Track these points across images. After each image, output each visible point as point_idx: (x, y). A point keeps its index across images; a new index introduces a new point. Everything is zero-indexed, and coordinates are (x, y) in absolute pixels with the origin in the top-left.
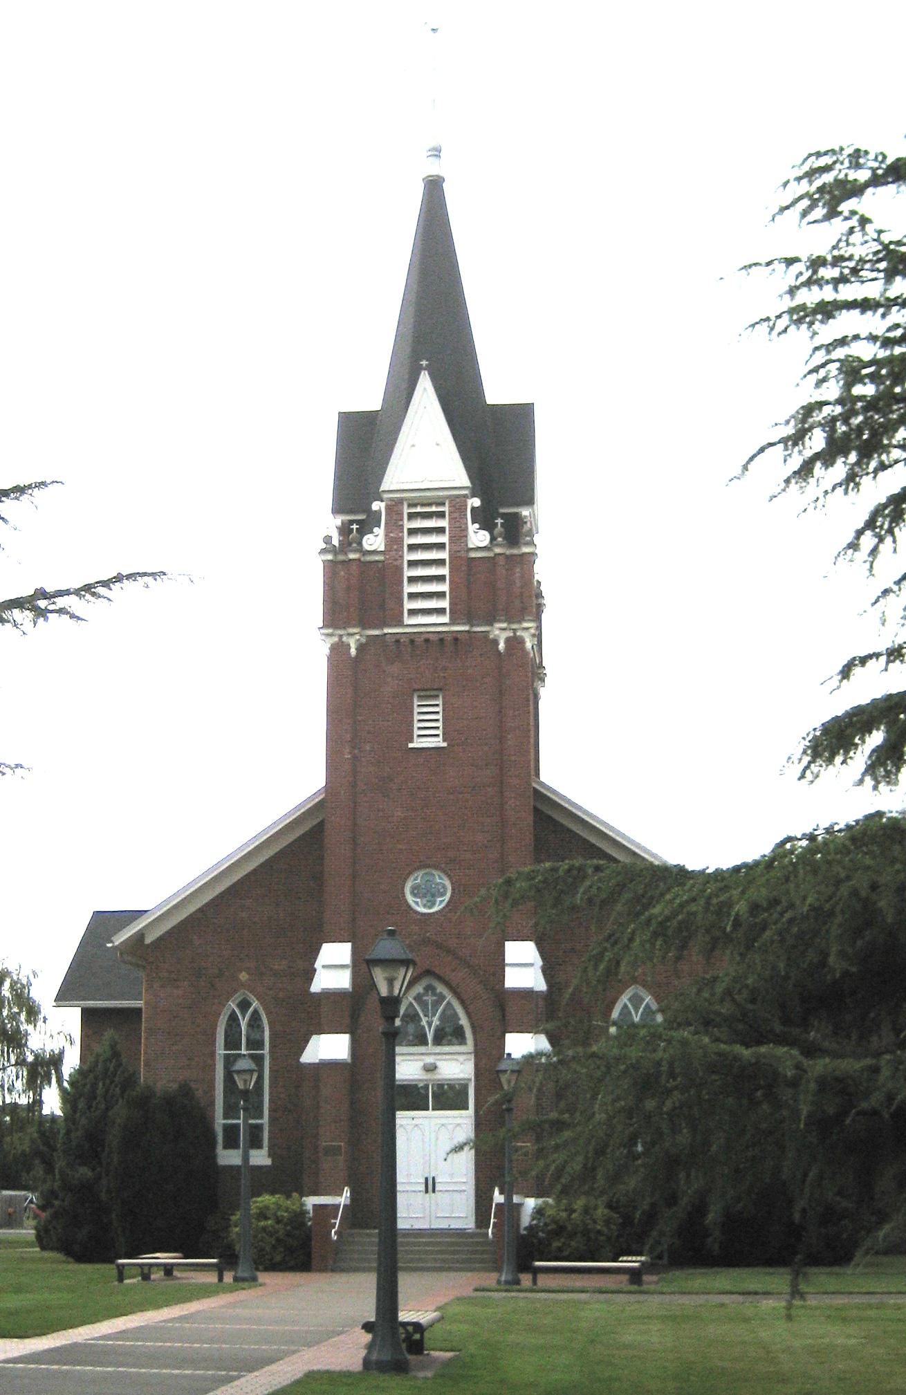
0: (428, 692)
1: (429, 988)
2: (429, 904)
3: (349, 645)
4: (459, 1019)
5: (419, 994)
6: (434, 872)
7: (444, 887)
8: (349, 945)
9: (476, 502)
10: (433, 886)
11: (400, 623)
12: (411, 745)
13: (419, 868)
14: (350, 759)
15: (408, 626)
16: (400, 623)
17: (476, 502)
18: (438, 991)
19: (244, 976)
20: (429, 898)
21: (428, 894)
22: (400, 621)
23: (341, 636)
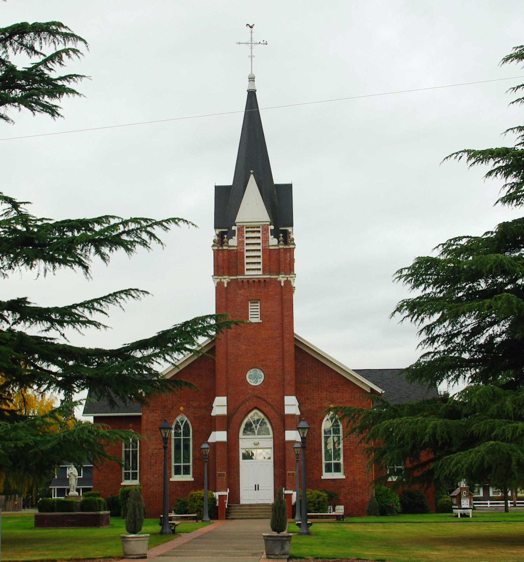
0: (254, 301)
3: (224, 283)
6: (258, 370)
7: (261, 375)
9: (272, 227)
19: (182, 409)
21: (256, 378)
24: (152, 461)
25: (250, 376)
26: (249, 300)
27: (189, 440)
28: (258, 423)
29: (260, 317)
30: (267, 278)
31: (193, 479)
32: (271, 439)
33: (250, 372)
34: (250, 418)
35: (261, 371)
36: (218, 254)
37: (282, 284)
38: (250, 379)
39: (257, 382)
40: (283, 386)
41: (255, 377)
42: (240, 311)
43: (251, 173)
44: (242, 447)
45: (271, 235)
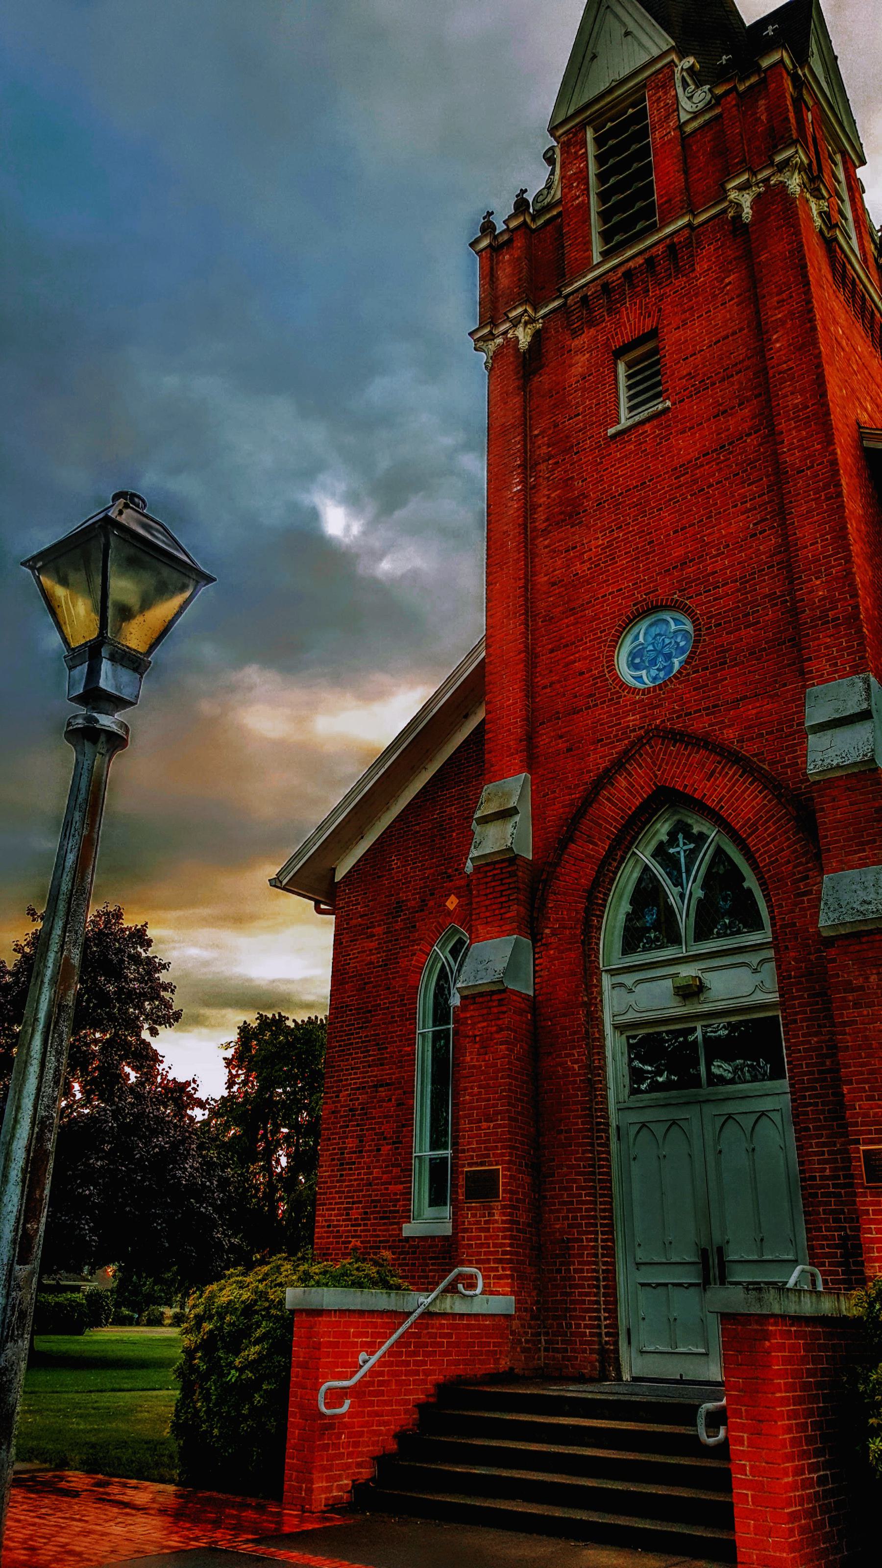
4: (743, 879)
6: (667, 616)
8: (749, 19)
10: (667, 641)
18: (695, 830)
19: (452, 903)
25: (633, 655)
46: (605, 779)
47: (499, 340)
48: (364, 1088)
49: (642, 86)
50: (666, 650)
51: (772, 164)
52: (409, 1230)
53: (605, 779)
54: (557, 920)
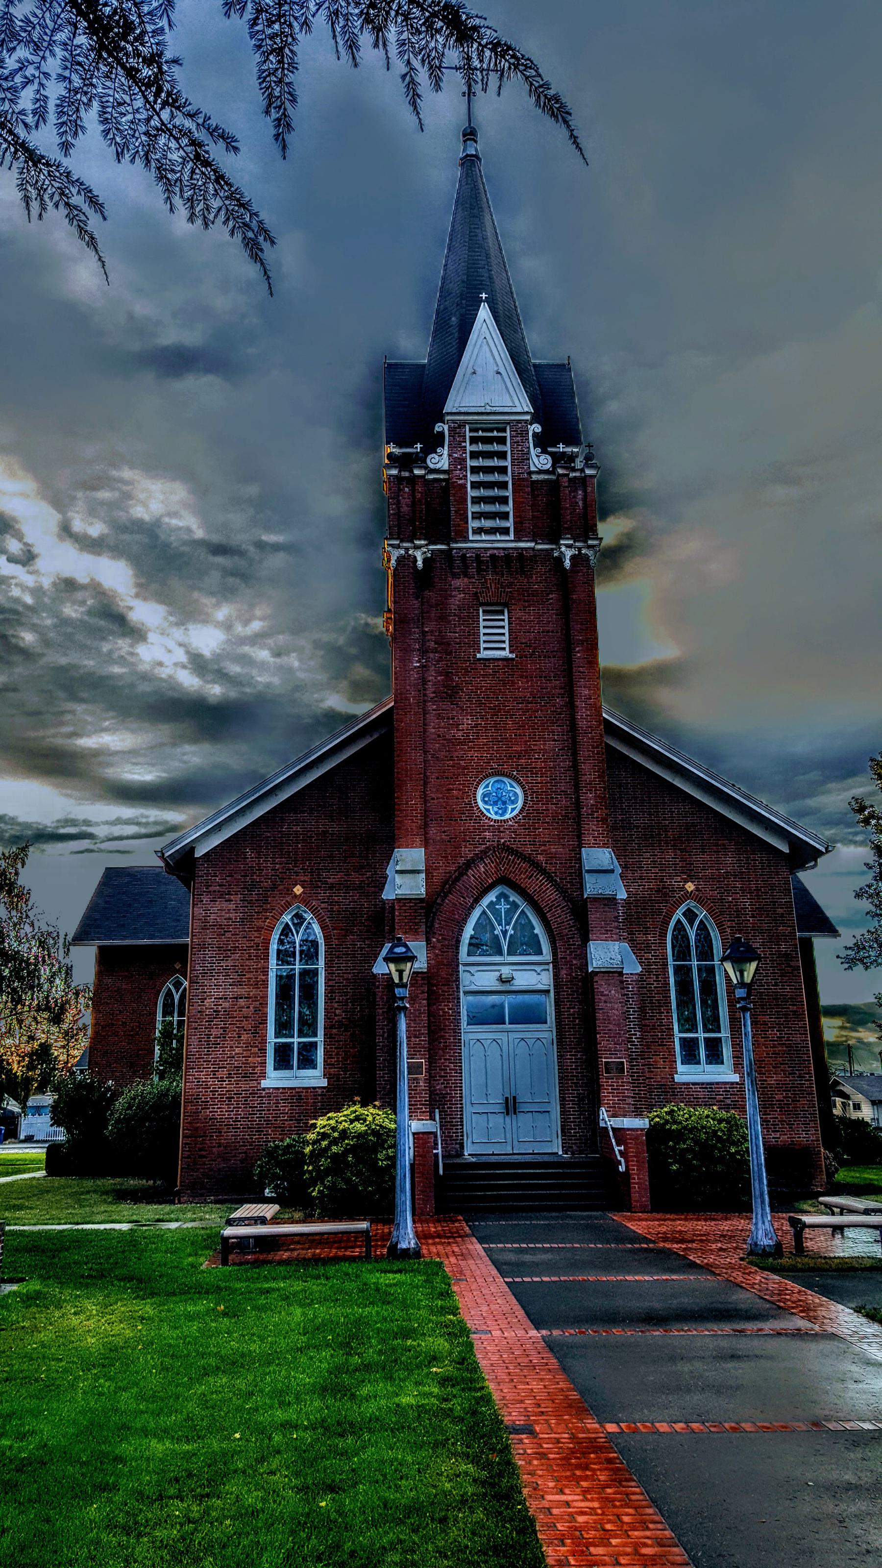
0: (495, 607)
1: (502, 895)
2: (500, 812)
3: (415, 557)
5: (492, 902)
6: (505, 780)
7: (516, 794)
9: (537, 428)
11: (466, 539)
12: (478, 656)
13: (487, 776)
14: (419, 667)
15: (472, 541)
16: (466, 539)
17: (537, 428)
18: (511, 899)
19: (298, 890)
20: (500, 805)
21: (501, 802)
22: (465, 537)
23: (407, 549)
24: (214, 1032)
25: (484, 796)
26: (482, 604)
27: (315, 972)
28: (508, 924)
29: (510, 646)
30: (526, 549)
31: (324, 1083)
32: (546, 967)
33: (487, 786)
34: (488, 907)
35: (515, 785)
36: (400, 490)
37: (567, 563)
38: (485, 802)
39: (505, 811)
40: (579, 817)
41: (500, 799)
42: (458, 629)
43: (481, 300)
44: (467, 989)
45: (535, 447)
46: (469, 864)
47: (402, 552)
48: (226, 998)
49: (508, 423)
50: (503, 799)
51: (586, 542)
52: (265, 1084)
53: (469, 864)
54: (440, 935)
